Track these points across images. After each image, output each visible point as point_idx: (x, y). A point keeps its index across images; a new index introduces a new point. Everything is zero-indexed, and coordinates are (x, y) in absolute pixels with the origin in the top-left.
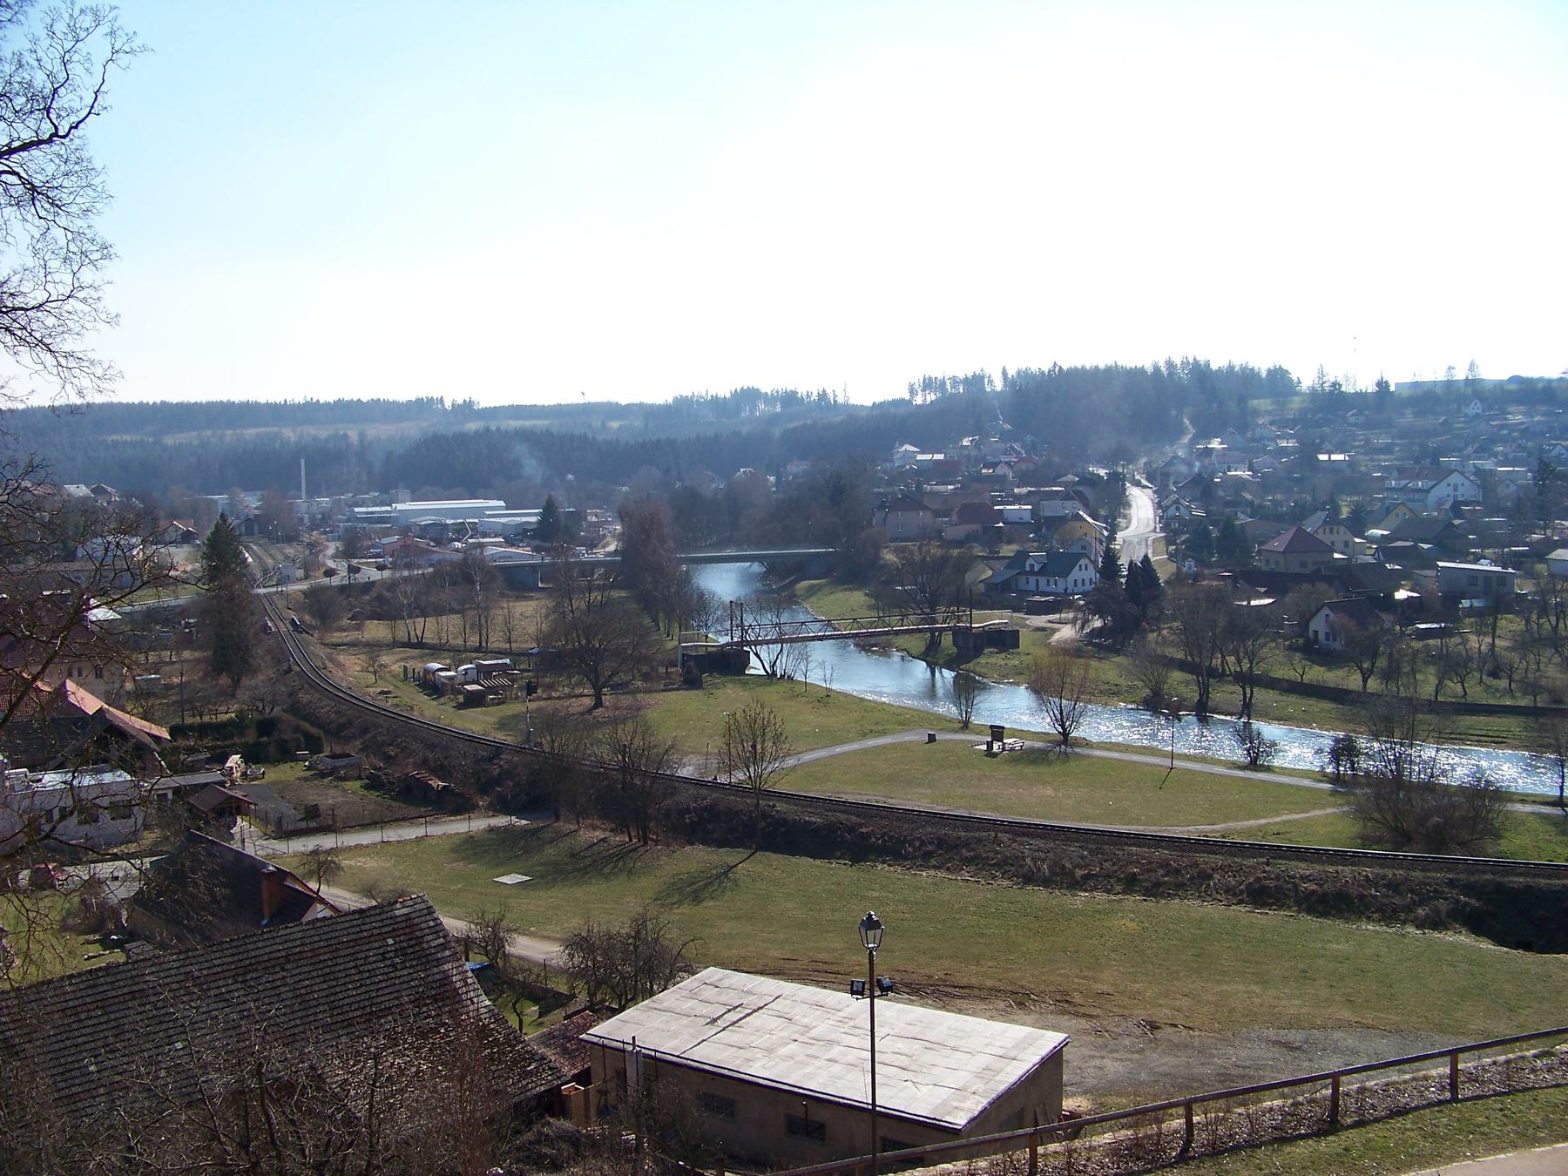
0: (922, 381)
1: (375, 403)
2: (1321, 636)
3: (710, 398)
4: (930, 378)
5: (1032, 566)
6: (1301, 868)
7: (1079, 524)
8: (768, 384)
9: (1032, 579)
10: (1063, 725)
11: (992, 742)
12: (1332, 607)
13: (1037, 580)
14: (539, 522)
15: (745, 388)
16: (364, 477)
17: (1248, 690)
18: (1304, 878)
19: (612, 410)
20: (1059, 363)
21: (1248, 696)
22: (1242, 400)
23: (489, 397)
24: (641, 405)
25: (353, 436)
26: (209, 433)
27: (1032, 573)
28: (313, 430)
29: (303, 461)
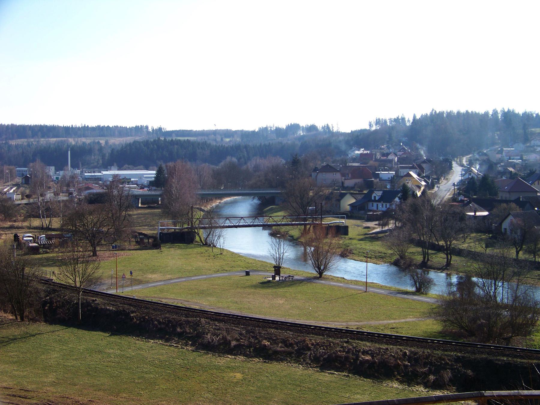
0: (375, 120)
1: (116, 127)
2: (508, 232)
3: (275, 128)
4: (379, 119)
5: (375, 197)
6: (366, 345)
7: (410, 178)
8: (304, 122)
9: (375, 204)
10: (319, 268)
11: (275, 275)
12: (515, 216)
13: (377, 205)
14: (155, 177)
15: (293, 124)
16: (101, 162)
17: (449, 256)
18: (365, 353)
19: (228, 133)
20: (435, 109)
21: (449, 258)
22: (525, 127)
23: (169, 127)
24: (242, 131)
25: (103, 142)
26: (32, 140)
27: (375, 201)
28: (84, 140)
29: (69, 152)
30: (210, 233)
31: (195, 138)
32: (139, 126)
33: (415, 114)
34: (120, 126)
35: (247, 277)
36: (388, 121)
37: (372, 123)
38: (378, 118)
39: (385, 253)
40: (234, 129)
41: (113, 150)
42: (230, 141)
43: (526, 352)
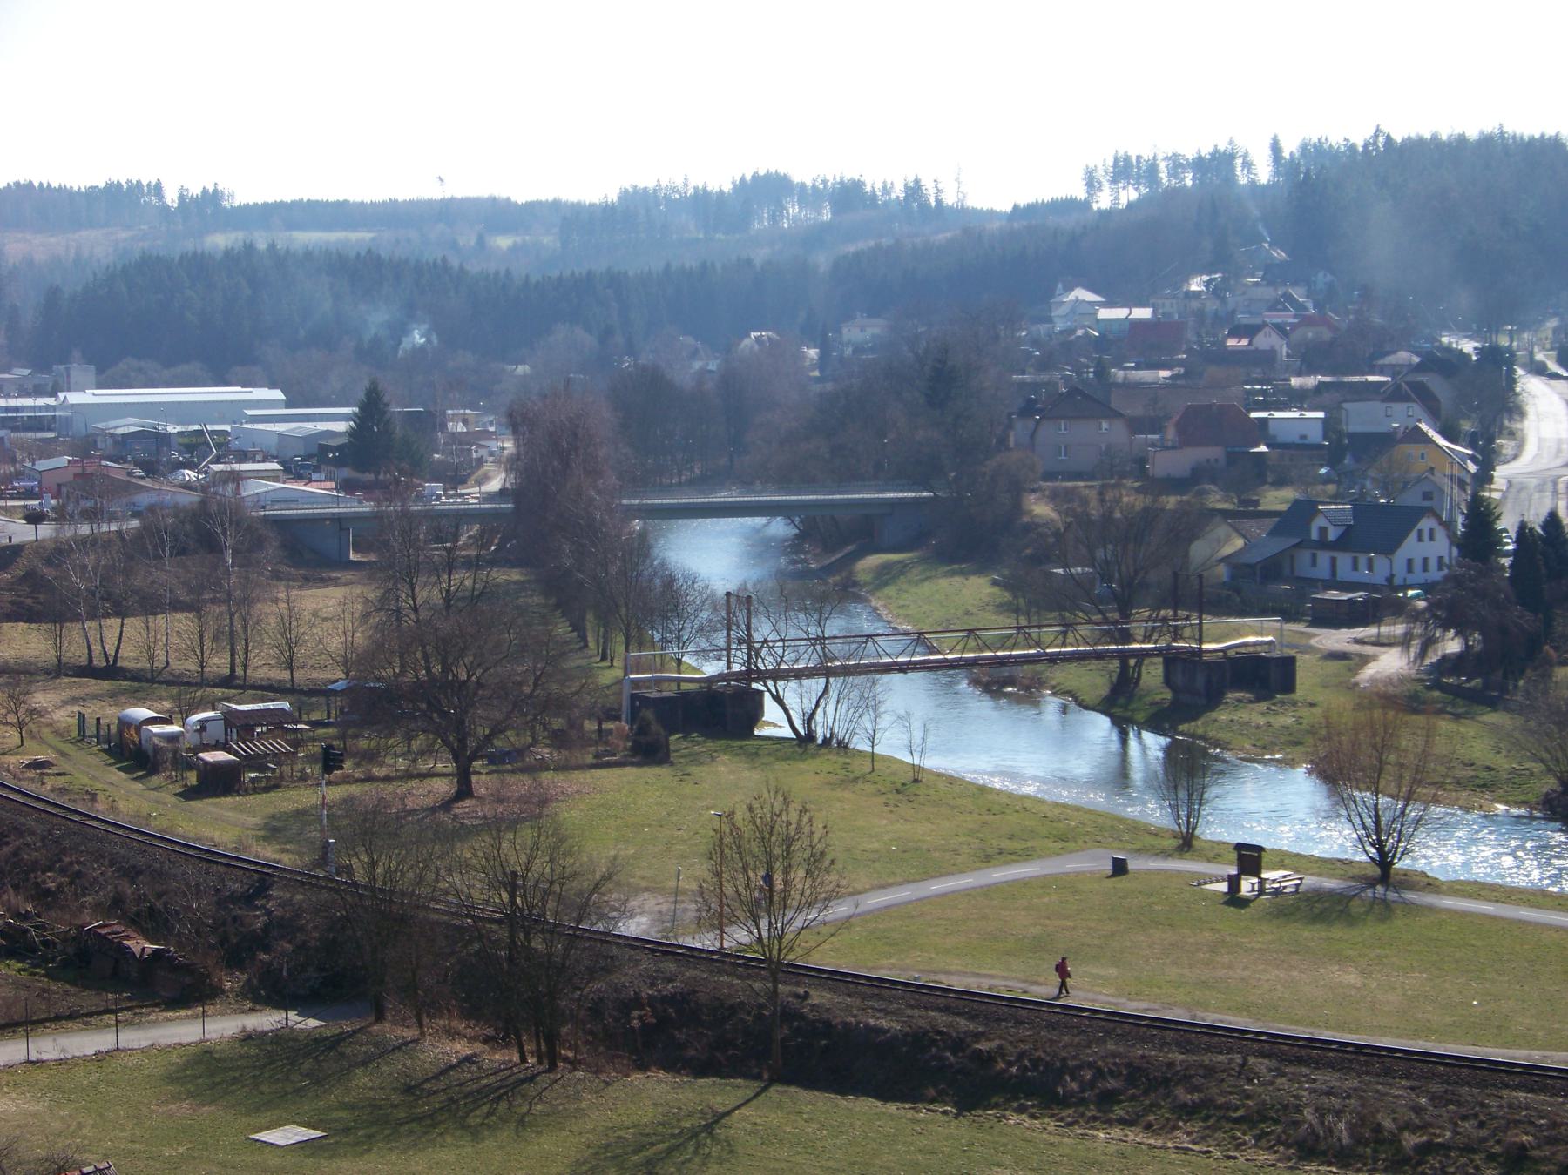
5: (1323, 530)
13: (1333, 561)
15: (762, 173)
19: (498, 214)
20: (1385, 128)
23: (246, 191)
27: (1323, 544)
30: (826, 690)
31: (367, 236)
32: (123, 182)
33: (1279, 138)
34: (41, 184)
35: (1121, 883)
36: (1162, 166)
37: (1100, 174)
38: (1121, 153)
39: (1489, 769)
40: (521, 197)
41: (53, 294)
42: (514, 249)
43: (239, 746)
